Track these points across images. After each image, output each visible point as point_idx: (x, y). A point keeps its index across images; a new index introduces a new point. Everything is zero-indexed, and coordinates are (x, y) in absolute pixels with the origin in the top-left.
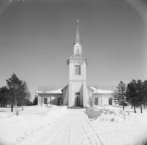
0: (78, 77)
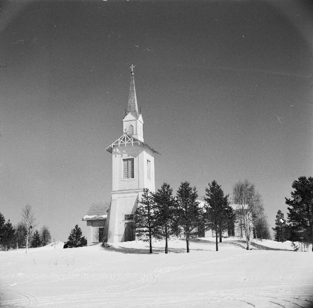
0: (131, 183)
